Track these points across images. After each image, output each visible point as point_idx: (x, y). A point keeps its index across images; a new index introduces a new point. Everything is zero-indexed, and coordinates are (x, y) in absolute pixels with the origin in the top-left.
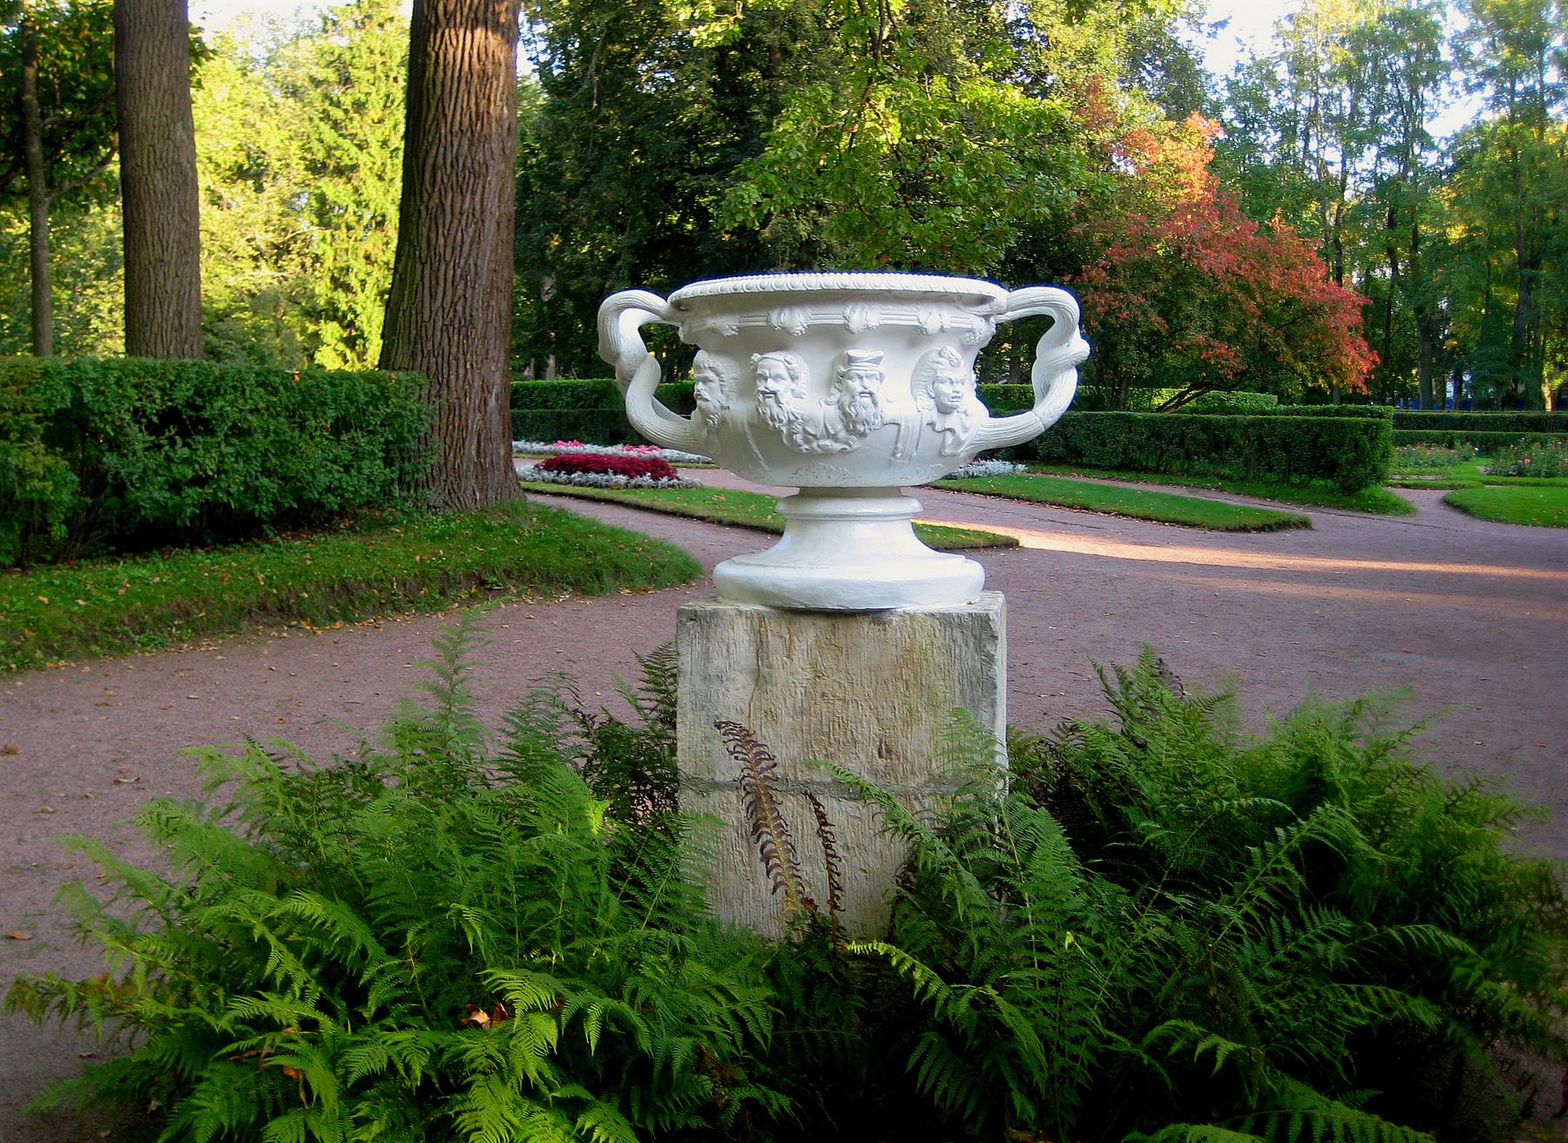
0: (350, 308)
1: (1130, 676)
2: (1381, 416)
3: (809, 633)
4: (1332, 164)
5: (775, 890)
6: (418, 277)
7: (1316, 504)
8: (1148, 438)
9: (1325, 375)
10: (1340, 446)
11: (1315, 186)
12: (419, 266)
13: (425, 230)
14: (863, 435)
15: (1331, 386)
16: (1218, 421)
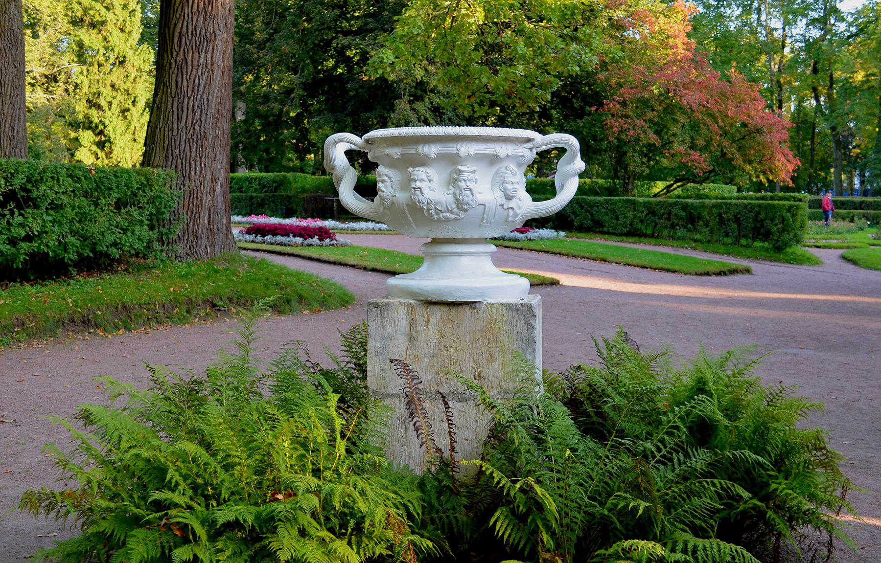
0: (101, 121)
1: (612, 343)
2: (800, 200)
3: (438, 313)
4: (776, 29)
5: (421, 446)
6: (169, 107)
7: (756, 258)
8: (647, 215)
9: (764, 173)
10: (772, 220)
11: (765, 44)
13: (174, 76)
14: (466, 210)
15: (768, 179)
16: (692, 204)
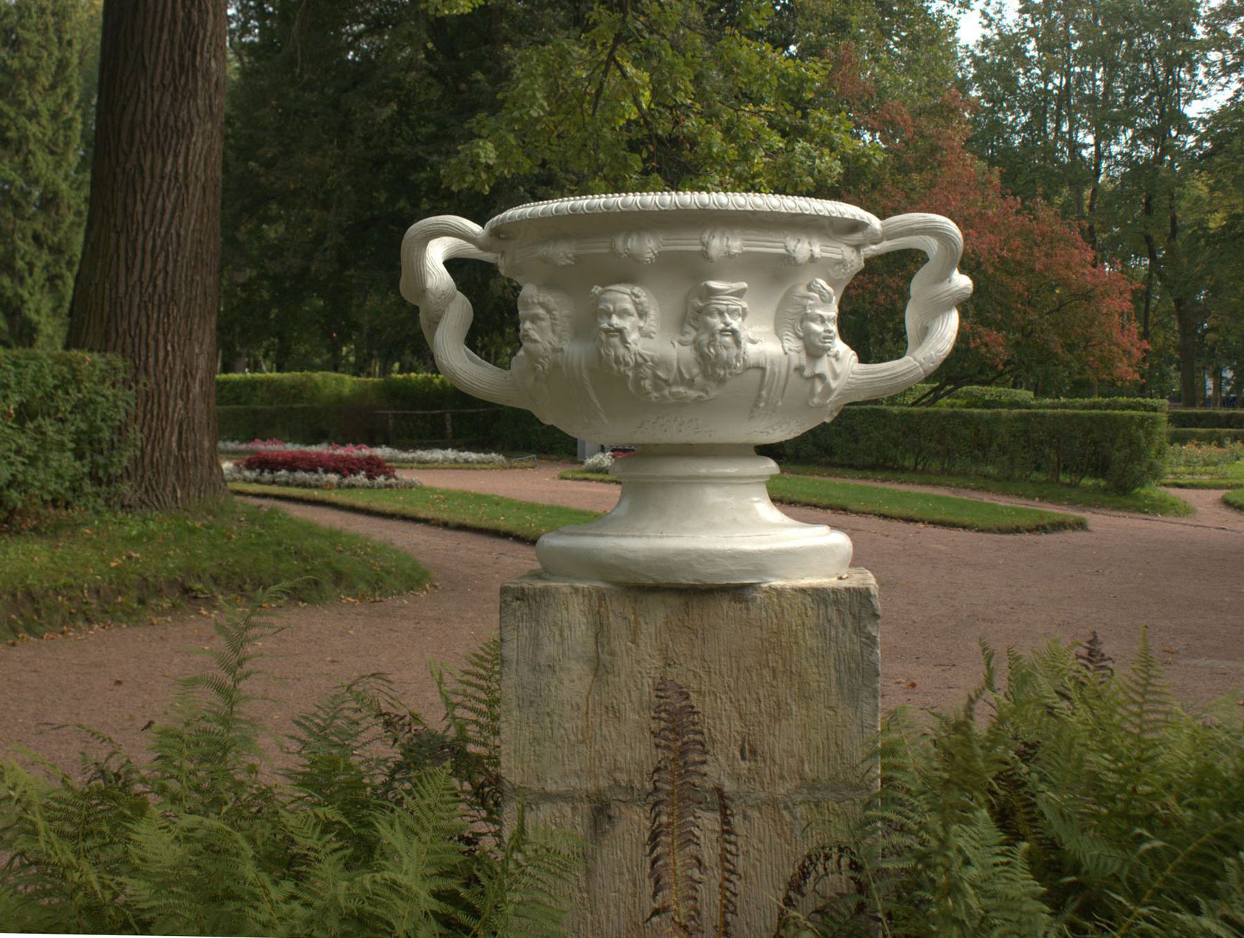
2: (1155, 410)
3: (658, 614)
12: (113, 235)
14: (722, 381)
